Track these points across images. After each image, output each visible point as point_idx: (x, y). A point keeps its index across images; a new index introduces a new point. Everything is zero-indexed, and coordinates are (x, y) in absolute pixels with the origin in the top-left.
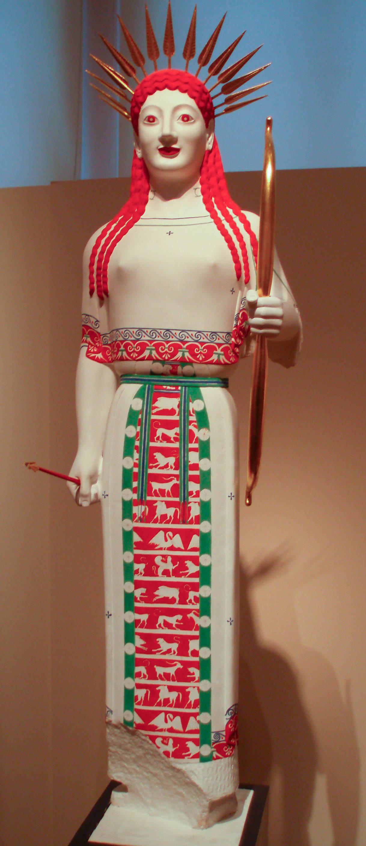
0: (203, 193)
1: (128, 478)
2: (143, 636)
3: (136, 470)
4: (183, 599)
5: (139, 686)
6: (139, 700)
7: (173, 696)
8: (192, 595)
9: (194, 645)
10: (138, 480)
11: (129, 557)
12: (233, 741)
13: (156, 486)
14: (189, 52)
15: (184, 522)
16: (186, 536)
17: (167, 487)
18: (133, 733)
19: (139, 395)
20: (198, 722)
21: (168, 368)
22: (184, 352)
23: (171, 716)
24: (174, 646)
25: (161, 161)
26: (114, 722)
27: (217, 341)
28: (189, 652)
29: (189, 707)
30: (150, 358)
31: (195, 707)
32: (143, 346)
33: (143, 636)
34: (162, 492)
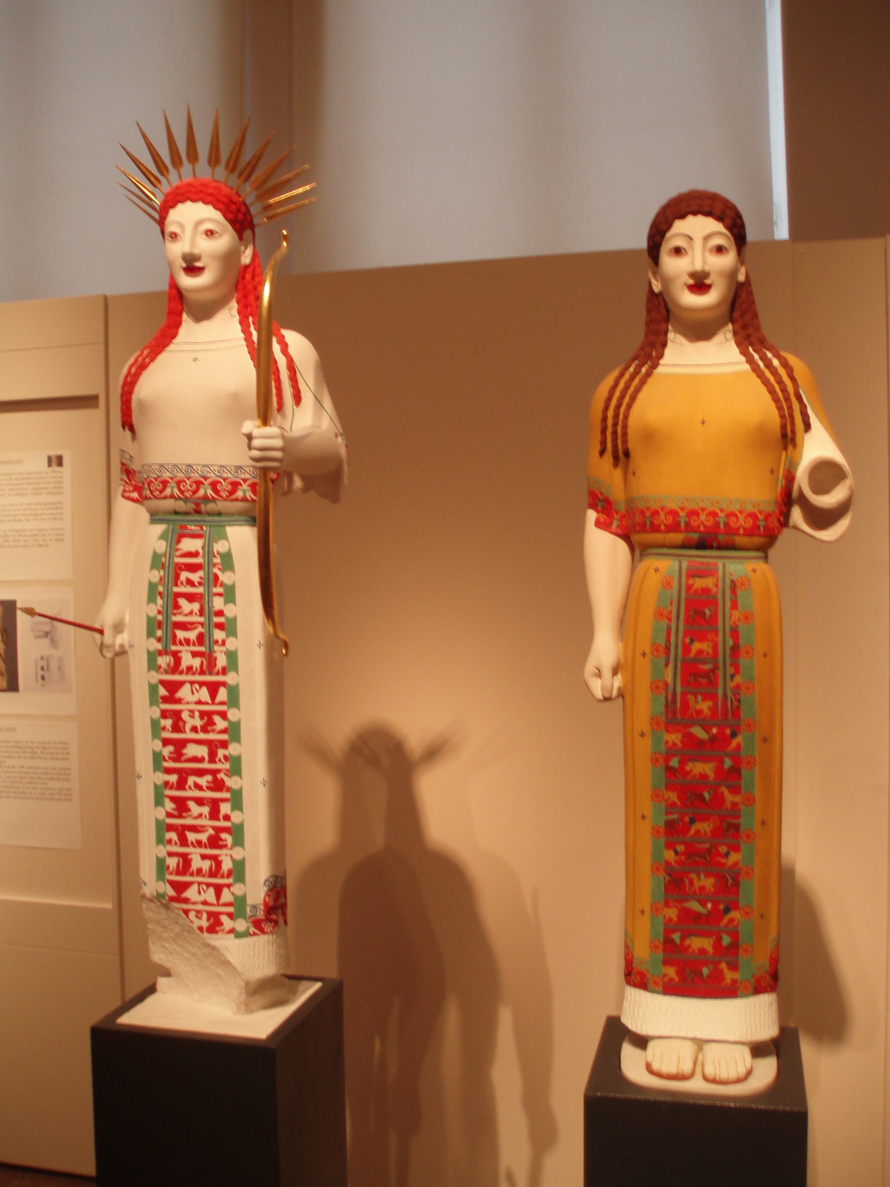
0: (239, 312)
1: (153, 625)
2: (173, 799)
3: (160, 617)
4: (212, 758)
5: (171, 854)
6: (171, 869)
7: (206, 865)
8: (221, 753)
9: (225, 808)
10: (164, 628)
11: (156, 713)
12: (274, 917)
13: (181, 634)
14: (214, 160)
15: (211, 674)
16: (213, 688)
17: (192, 635)
18: (167, 907)
19: (163, 537)
20: (233, 894)
21: (191, 506)
22: (172, 488)
23: (205, 887)
24: (205, 810)
25: (187, 282)
26: (148, 894)
27: (243, 476)
28: (221, 817)
29: (222, 877)
30: (172, 496)
31: (228, 877)
32: (165, 483)
33: (173, 799)
34: (188, 641)
